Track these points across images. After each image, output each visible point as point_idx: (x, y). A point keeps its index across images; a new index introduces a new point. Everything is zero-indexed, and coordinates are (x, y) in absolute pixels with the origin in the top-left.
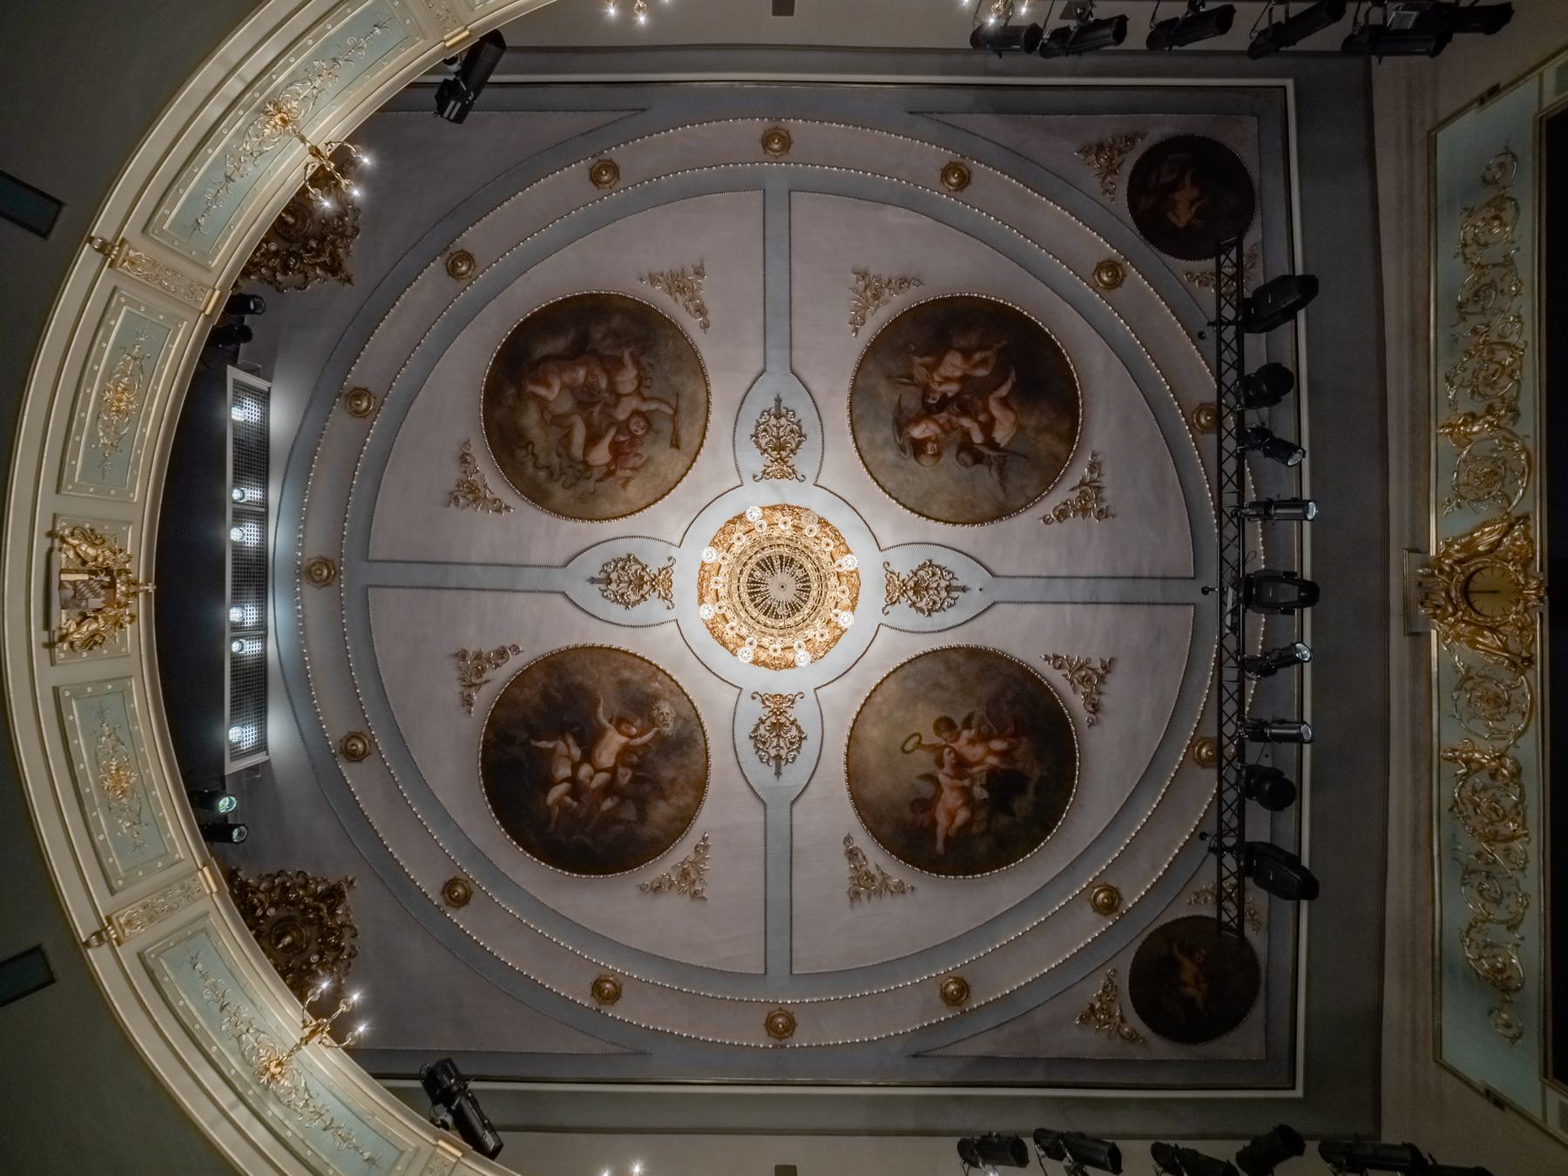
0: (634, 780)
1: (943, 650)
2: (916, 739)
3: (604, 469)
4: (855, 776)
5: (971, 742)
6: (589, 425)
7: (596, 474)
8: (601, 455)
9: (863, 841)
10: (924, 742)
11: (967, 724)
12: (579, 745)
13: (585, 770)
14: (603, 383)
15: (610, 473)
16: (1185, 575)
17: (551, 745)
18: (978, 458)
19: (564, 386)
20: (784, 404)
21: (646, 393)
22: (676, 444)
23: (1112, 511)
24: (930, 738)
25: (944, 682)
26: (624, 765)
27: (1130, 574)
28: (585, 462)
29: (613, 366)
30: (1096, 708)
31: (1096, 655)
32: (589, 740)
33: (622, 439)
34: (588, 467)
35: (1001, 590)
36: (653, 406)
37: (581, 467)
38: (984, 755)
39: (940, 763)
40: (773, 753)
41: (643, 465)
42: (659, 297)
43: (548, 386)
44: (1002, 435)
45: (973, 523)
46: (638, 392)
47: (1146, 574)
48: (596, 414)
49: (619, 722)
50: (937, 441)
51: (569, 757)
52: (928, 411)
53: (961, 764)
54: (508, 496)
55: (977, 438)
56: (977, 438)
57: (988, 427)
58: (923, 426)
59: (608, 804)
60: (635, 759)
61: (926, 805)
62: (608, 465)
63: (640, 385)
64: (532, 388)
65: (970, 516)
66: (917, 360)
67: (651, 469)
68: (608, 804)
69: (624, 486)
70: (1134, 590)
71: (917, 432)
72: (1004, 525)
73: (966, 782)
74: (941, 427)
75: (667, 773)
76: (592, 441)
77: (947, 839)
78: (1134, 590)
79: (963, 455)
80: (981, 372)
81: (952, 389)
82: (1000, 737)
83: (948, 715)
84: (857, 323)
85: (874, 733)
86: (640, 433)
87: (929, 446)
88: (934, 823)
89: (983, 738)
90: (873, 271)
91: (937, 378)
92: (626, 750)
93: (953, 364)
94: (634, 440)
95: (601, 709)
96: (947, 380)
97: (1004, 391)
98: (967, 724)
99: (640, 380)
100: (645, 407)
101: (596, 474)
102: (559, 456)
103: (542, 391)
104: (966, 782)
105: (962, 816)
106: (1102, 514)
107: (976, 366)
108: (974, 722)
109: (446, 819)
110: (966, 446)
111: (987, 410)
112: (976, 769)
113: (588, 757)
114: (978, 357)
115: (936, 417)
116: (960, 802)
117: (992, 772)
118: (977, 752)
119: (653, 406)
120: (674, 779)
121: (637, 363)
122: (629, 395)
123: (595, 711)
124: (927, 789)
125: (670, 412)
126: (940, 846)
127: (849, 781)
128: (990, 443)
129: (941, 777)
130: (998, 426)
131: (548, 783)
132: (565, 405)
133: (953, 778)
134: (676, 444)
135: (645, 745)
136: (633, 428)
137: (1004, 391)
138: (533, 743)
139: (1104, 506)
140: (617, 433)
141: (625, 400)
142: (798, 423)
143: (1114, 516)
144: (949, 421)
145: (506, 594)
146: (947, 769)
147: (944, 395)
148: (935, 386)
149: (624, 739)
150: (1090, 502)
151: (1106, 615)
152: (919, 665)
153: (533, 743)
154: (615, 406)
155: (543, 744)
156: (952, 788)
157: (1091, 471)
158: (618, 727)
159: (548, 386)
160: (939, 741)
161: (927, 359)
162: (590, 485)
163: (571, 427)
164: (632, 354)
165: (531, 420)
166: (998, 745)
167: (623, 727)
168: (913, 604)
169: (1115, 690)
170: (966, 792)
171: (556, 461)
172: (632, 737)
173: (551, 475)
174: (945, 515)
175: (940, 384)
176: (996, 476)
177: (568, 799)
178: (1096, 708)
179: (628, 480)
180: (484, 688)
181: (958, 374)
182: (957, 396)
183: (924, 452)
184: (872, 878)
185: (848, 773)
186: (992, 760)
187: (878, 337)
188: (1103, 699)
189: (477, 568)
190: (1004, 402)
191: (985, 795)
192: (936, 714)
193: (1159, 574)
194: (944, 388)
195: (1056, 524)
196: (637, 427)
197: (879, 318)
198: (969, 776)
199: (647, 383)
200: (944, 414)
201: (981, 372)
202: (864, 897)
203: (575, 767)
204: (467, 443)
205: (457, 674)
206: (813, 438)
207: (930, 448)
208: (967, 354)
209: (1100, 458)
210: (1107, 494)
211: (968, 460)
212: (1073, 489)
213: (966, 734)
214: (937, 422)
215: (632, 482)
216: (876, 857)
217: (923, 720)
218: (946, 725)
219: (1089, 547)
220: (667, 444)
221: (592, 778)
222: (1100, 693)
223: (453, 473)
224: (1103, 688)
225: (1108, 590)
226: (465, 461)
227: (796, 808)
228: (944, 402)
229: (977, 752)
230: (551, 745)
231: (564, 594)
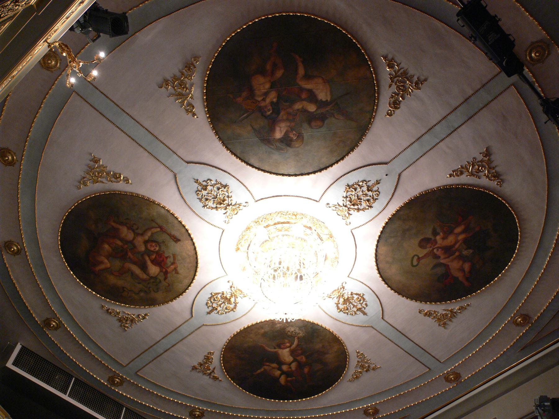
0: (307, 357)
1: (394, 215)
2: (416, 258)
3: (162, 274)
4: (400, 290)
5: (444, 239)
6: (135, 263)
7: (161, 277)
8: (154, 270)
9: (427, 307)
10: (420, 256)
11: (435, 233)
12: (273, 363)
13: (285, 368)
14: (119, 243)
15: (166, 273)
16: (495, 73)
17: (262, 370)
18: (322, 118)
19: (108, 257)
20: (201, 180)
21: (140, 231)
22: (177, 240)
23: (422, 78)
24: (422, 253)
25: (407, 227)
26: (298, 356)
27: (462, 100)
28: (152, 277)
29: (115, 234)
30: (497, 176)
31: (476, 153)
32: (276, 359)
33: (154, 257)
34: (155, 278)
35: (397, 166)
36: (149, 234)
37: (152, 281)
38: (457, 237)
39: (437, 257)
40: (355, 309)
41: (174, 259)
42: (94, 188)
43: (102, 262)
44: (323, 95)
45: (352, 150)
46: (137, 235)
47: (471, 92)
48: (132, 256)
49: (279, 346)
50: (292, 129)
51: (273, 368)
52: (273, 123)
53: (448, 250)
54: (142, 311)
55: (312, 108)
56: (312, 108)
57: (312, 97)
58: (278, 129)
59: (306, 370)
60: (300, 352)
61: (447, 274)
62: (161, 271)
63: (133, 231)
64: (98, 268)
65: (347, 149)
66: (239, 100)
67: (179, 258)
68: (306, 370)
69: (177, 273)
70: (468, 108)
71: (278, 134)
72: (369, 137)
73: (457, 254)
74: (287, 120)
75: (318, 346)
76: (144, 268)
77: (467, 279)
78: (468, 108)
79: (313, 124)
80: (279, 73)
81: (273, 96)
82: (458, 225)
83: (421, 237)
84: (190, 109)
85: (393, 271)
86: (157, 249)
87: (291, 135)
88: (456, 278)
89: (449, 232)
90: (168, 76)
91: (260, 99)
92: (292, 353)
93: (261, 84)
94: (159, 254)
95: (266, 348)
96: (266, 94)
97: (301, 71)
98: (435, 233)
99: (130, 228)
100: (146, 238)
101: (161, 277)
102: (139, 283)
103: (102, 267)
104: (457, 254)
105: (467, 266)
106: (418, 85)
107: (273, 73)
108: (438, 230)
109: (255, 411)
110: (311, 119)
111: (302, 90)
112: (457, 246)
113: (281, 363)
114: (268, 67)
115: (280, 117)
116: (461, 263)
117: (465, 241)
118: (451, 239)
119: (149, 234)
120: (323, 346)
121: (122, 224)
122: (134, 239)
123: (266, 350)
124: (440, 271)
125: (159, 229)
126: (466, 283)
127: (399, 294)
128: (321, 104)
129: (442, 261)
130: (317, 92)
131: (277, 379)
132: (117, 264)
133: (448, 257)
134: (177, 240)
135: (298, 345)
136: (152, 249)
137: (301, 71)
138: (255, 373)
139: (415, 79)
140: (149, 257)
141: (135, 241)
142: (217, 183)
143: (426, 80)
144: (289, 114)
145: (184, 341)
146: (442, 257)
147: (272, 103)
148: (263, 104)
149: (288, 350)
150: (404, 82)
151: (465, 131)
152: (387, 230)
153: (255, 373)
154: (135, 247)
155: (259, 371)
156: (452, 261)
157: (391, 66)
158: (280, 348)
159: (102, 262)
160: (425, 251)
161: (244, 94)
162: (164, 283)
163: (129, 270)
164: (114, 222)
165: (112, 280)
166: (458, 230)
167: (282, 346)
168: (358, 210)
169: (500, 160)
170: (461, 258)
171: (140, 286)
172: (290, 347)
173: (145, 292)
174: (334, 160)
175: (264, 100)
176: (341, 118)
177: (289, 379)
178: (497, 176)
179: (175, 269)
180: (215, 371)
181: (268, 86)
182: (279, 97)
183: (291, 140)
184: (447, 315)
185: (396, 292)
186: (461, 237)
187: (209, 112)
188: (498, 169)
189: (163, 340)
190: (308, 77)
191: (471, 251)
192: (416, 241)
193: (479, 87)
194: (268, 100)
195: (397, 111)
196: (154, 248)
197: (196, 94)
198: (457, 250)
199: (135, 227)
200: (282, 113)
201: (279, 73)
202: (448, 322)
203: (280, 369)
204: (103, 307)
205: (201, 374)
206: (231, 182)
207: (293, 136)
208: (262, 72)
209: (390, 57)
210: (411, 72)
211: (319, 123)
212: (390, 86)
213: (438, 238)
214: (283, 120)
215: (178, 269)
216: (440, 308)
217: (412, 247)
218: (424, 243)
219: (423, 105)
220: (174, 243)
221: (290, 368)
222: (494, 168)
223: (113, 320)
224: (493, 165)
225: (456, 119)
226: (111, 313)
227: (386, 318)
228: (276, 108)
229: (451, 239)
230: (262, 370)
231: (203, 325)
